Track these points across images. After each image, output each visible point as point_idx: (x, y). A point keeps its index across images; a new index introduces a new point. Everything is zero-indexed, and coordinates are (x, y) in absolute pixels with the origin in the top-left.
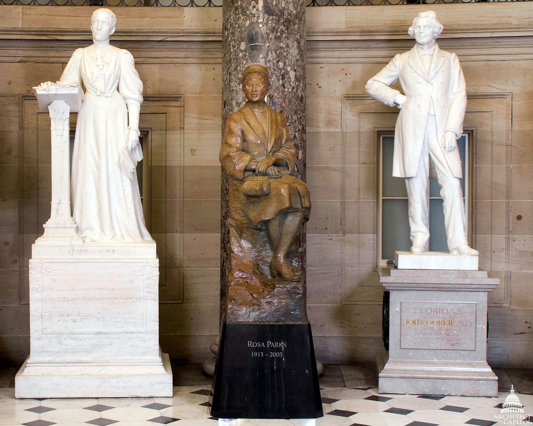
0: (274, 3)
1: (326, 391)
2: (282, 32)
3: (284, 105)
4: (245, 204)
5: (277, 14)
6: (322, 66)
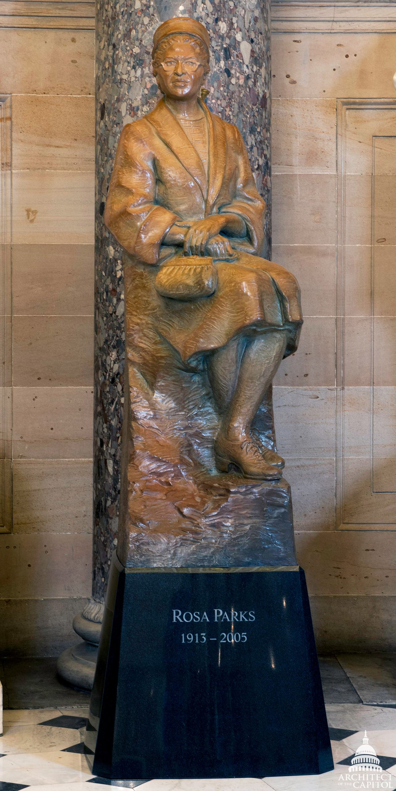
1: (336, 715)
3: (228, 112)
4: (162, 315)
6: (297, 37)
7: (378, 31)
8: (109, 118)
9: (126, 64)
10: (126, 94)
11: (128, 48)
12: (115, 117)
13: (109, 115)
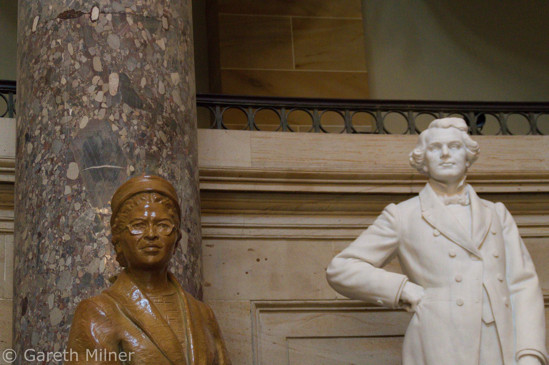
0: (143, 82)
2: (161, 145)
5: (149, 108)
7: (286, 237)
8: (32, 312)
9: (54, 253)
10: (53, 285)
11: (57, 236)
12: (40, 310)
13: (32, 309)
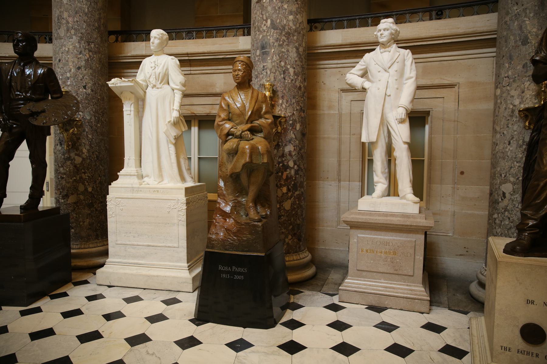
0: (278, 21)
3: (284, 91)
5: (280, 29)
